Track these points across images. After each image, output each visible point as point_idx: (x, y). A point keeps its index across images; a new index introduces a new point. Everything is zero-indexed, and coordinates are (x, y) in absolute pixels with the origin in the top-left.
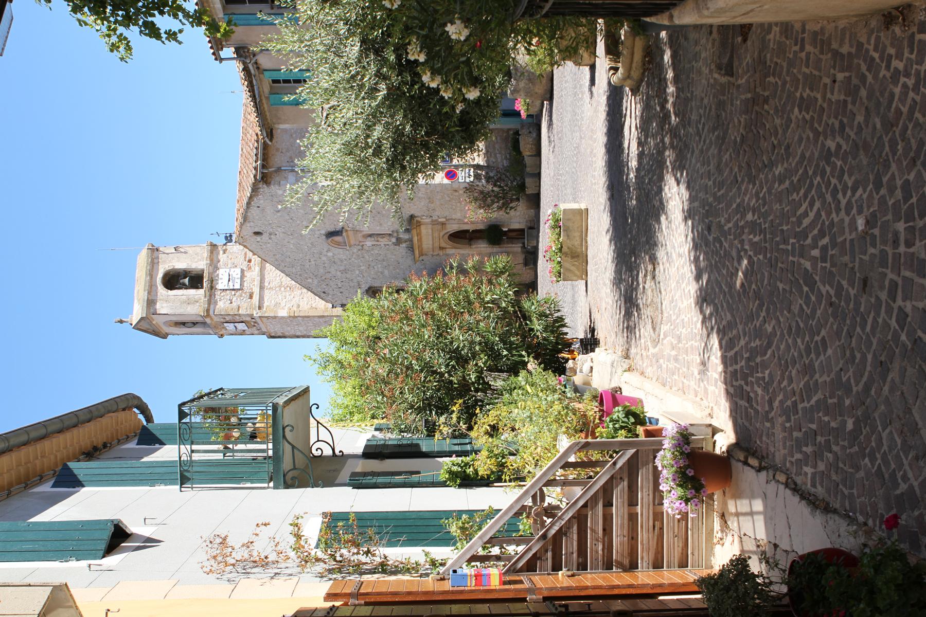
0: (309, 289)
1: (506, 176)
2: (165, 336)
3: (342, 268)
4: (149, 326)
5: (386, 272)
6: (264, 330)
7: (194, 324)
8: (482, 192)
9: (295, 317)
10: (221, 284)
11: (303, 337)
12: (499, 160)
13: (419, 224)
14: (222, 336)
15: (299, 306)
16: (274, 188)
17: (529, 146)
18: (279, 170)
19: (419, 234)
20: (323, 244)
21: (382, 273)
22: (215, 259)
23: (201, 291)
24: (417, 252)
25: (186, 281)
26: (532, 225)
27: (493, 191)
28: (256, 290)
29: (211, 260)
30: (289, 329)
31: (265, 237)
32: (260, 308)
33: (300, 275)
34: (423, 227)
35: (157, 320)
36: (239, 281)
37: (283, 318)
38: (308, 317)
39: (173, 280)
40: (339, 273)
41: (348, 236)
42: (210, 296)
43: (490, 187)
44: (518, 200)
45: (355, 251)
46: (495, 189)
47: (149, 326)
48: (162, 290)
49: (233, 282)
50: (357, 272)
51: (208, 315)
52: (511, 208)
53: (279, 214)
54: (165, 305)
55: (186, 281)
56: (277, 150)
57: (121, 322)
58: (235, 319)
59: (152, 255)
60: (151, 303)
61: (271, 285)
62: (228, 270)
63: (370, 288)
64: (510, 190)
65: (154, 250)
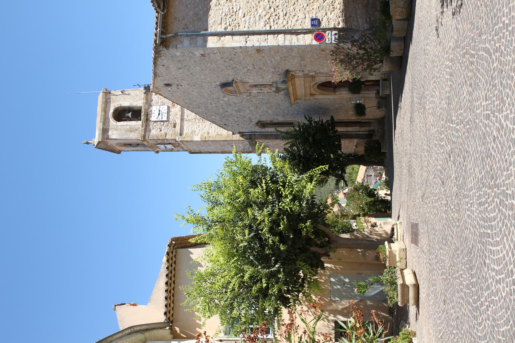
0: (213, 122)
1: (370, 39)
2: (119, 152)
3: (236, 109)
4: (104, 145)
5: (270, 111)
6: (186, 149)
7: (138, 145)
8: (347, 55)
9: (205, 141)
10: (153, 118)
11: (214, 153)
12: (360, 24)
13: (293, 77)
14: (157, 152)
15: (208, 133)
16: (172, 51)
17: (399, 10)
18: (176, 35)
19: (294, 85)
20: (219, 92)
21: (267, 112)
22: (149, 99)
23: (140, 123)
24: (292, 98)
25: (130, 115)
26: (386, 77)
27: (358, 54)
28: (178, 122)
29: (147, 100)
30: (203, 148)
31: (174, 88)
32: (181, 135)
33: (206, 114)
34: (296, 79)
35: (110, 143)
36: (166, 115)
37: (197, 141)
38: (216, 141)
39: (121, 114)
40: (234, 112)
41: (238, 87)
42: (146, 126)
43: (355, 50)
44: (381, 61)
45: (245, 96)
46: (361, 52)
47: (104, 145)
48: (112, 122)
49: (162, 116)
50: (248, 111)
51: (145, 140)
52: (375, 69)
53: (181, 71)
54: (115, 132)
55: (130, 115)
56: (175, 18)
57: (88, 143)
58: (164, 142)
59: (106, 96)
60: (105, 131)
61: (189, 118)
62: (158, 107)
63: (259, 122)
64: (375, 53)
65: (107, 93)
